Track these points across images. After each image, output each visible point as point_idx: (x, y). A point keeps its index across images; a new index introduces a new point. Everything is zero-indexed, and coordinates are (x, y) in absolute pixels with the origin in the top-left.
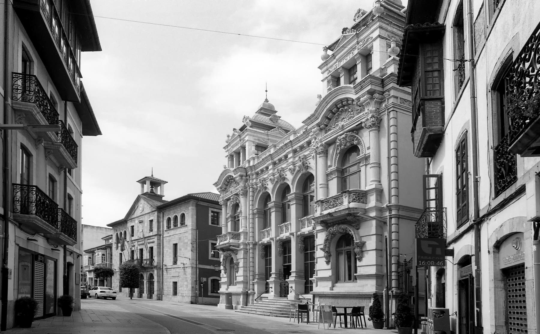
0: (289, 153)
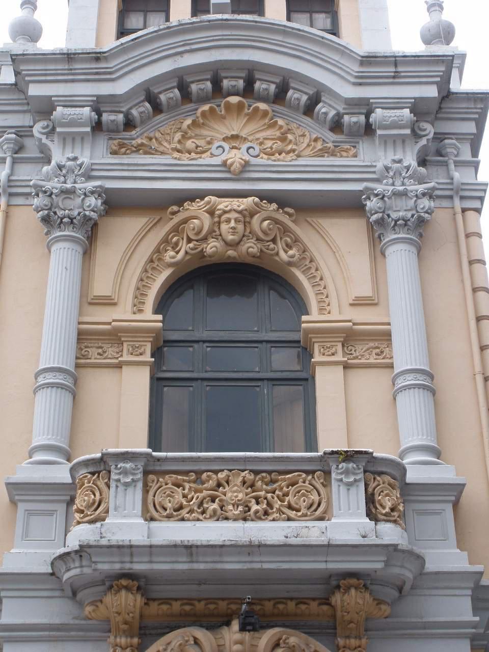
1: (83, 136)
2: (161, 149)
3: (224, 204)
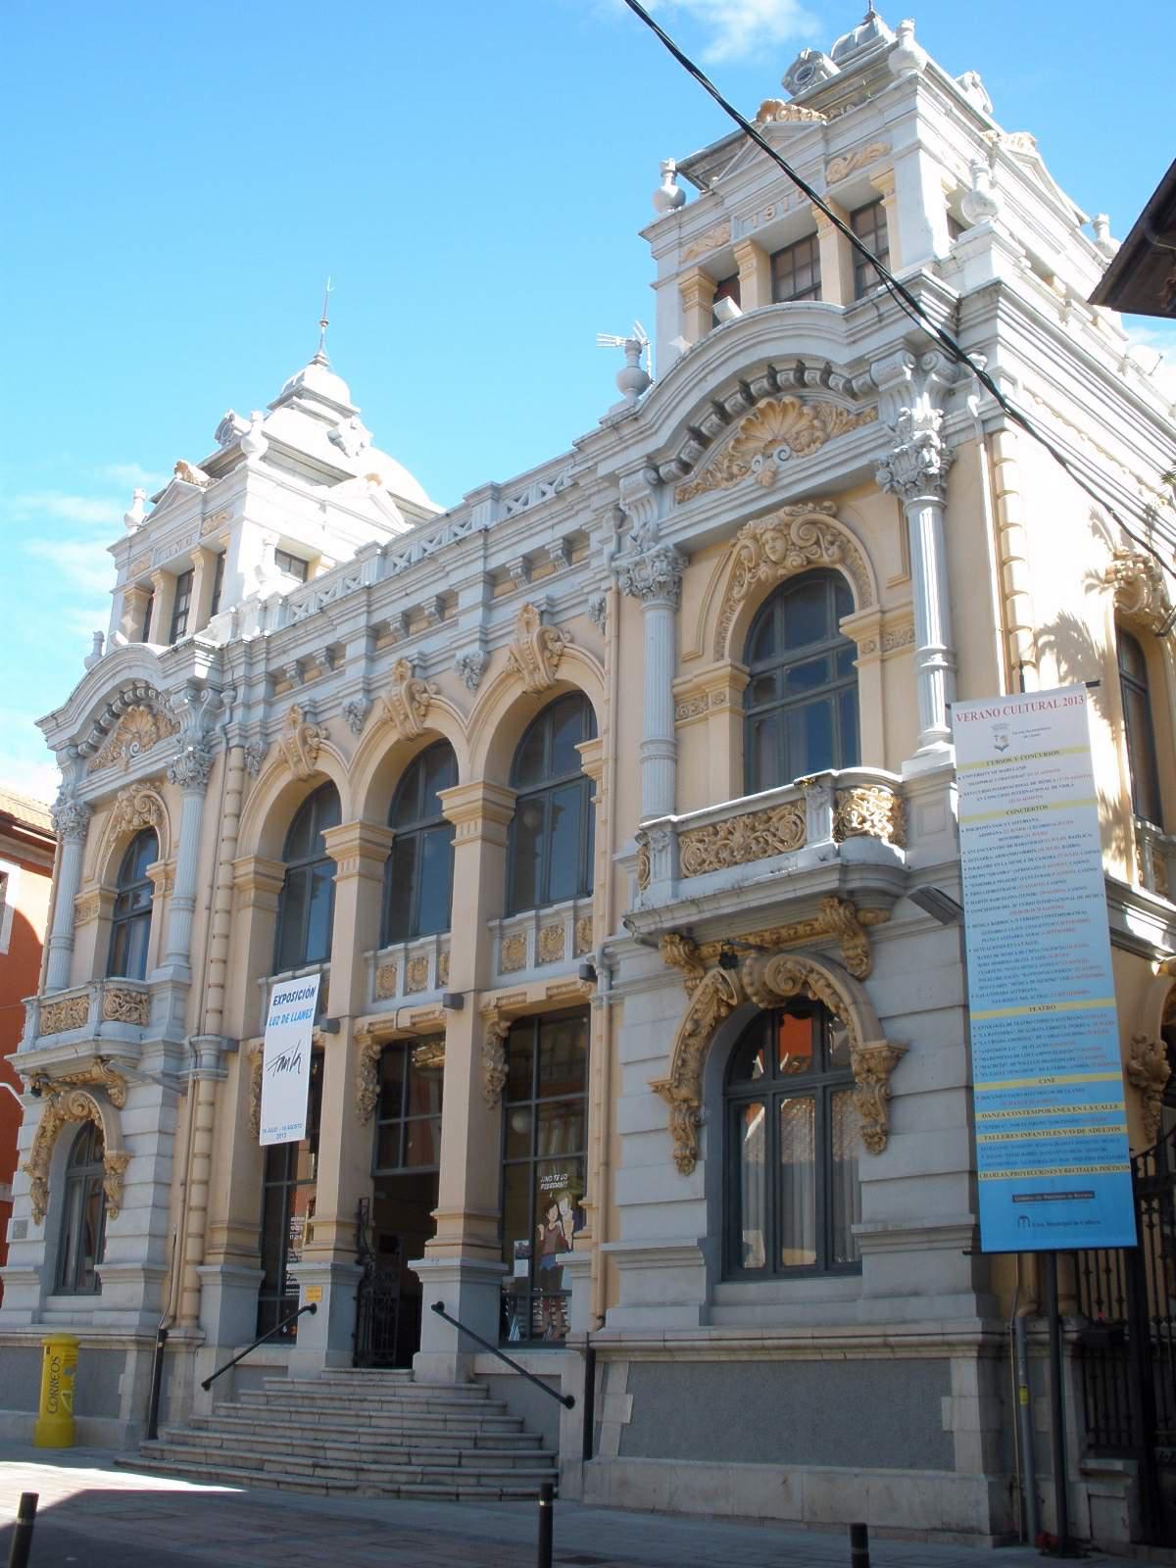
0: (468, 583)
1: (647, 498)
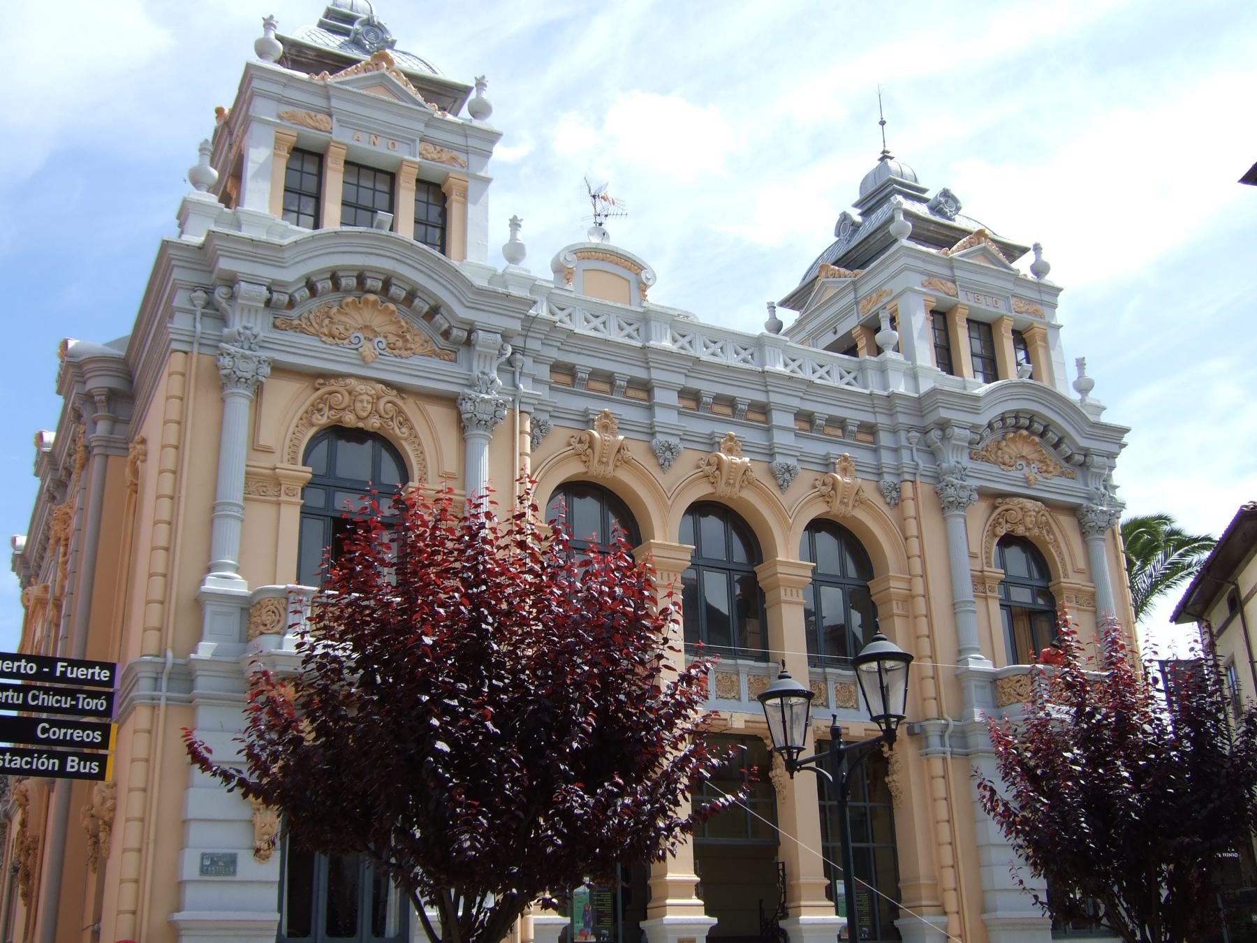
2: (312, 330)
3: (360, 387)
